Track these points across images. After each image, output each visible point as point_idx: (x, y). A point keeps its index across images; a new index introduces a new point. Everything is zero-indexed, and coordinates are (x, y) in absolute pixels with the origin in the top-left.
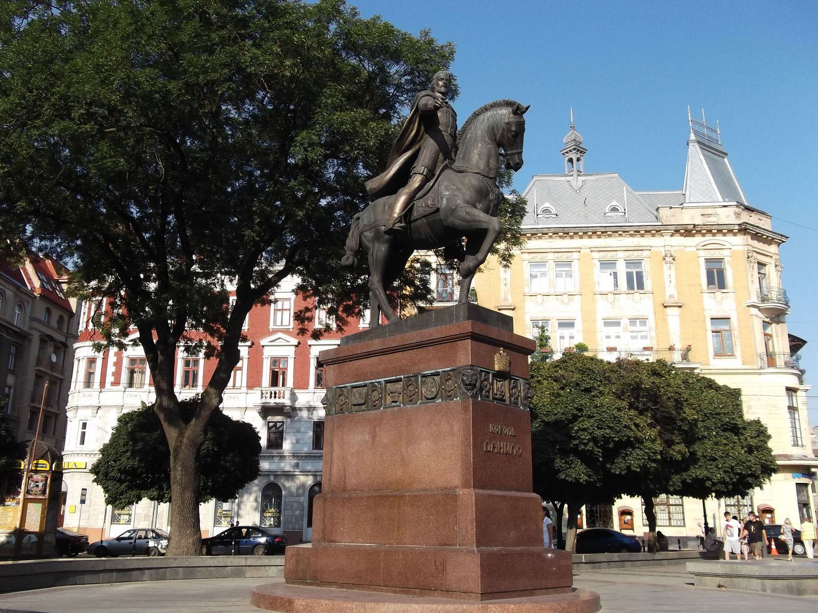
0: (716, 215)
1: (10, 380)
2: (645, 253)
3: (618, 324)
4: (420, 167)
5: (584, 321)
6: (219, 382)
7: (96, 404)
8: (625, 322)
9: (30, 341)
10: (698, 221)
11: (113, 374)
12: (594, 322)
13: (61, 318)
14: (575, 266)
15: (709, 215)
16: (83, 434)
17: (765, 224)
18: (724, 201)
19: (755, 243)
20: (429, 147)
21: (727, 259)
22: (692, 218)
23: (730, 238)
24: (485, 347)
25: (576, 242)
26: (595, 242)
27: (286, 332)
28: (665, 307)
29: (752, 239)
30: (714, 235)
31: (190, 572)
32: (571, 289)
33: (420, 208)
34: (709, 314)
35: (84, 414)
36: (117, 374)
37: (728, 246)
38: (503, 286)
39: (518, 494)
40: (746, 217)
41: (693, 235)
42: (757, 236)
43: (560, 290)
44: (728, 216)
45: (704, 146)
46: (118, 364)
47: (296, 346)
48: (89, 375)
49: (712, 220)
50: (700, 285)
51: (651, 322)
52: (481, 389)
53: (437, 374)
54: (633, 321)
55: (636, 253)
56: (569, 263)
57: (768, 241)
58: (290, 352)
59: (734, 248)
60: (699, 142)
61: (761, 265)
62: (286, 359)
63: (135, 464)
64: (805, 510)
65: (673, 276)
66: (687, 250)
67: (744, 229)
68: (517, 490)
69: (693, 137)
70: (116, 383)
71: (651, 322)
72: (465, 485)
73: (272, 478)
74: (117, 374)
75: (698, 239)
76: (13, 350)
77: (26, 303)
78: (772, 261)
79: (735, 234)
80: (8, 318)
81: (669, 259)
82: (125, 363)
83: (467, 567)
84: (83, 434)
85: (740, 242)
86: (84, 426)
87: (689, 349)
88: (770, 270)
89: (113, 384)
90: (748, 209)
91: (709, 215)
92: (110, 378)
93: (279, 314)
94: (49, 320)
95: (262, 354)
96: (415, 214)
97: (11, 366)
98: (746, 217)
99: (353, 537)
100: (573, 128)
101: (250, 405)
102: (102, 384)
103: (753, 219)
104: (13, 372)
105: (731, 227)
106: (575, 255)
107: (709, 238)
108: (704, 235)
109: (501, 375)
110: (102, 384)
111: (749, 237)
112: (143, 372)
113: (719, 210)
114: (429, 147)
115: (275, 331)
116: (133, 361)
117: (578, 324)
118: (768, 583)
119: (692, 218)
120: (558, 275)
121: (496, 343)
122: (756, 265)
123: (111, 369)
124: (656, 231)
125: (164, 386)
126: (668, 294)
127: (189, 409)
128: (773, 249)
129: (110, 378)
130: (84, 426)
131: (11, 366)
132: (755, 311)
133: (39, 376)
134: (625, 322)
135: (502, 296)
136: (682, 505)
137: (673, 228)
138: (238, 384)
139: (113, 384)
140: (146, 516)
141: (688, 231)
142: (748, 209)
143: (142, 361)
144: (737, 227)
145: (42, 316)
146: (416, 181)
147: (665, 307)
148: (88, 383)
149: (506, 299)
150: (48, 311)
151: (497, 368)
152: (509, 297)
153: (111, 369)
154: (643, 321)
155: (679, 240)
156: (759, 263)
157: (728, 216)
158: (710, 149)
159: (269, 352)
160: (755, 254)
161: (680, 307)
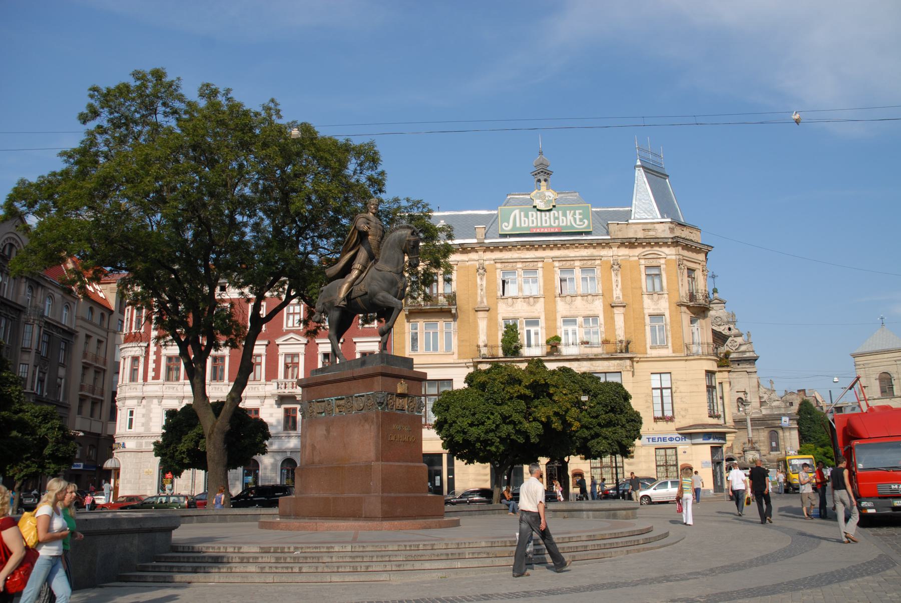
0: (655, 230)
1: (62, 372)
2: (598, 262)
3: (574, 322)
4: (357, 265)
5: (546, 319)
6: (240, 383)
7: (140, 394)
8: (580, 320)
9: (77, 337)
10: (640, 235)
11: (154, 370)
12: (555, 320)
13: (102, 315)
14: (540, 272)
15: (649, 230)
16: (131, 420)
17: (696, 237)
18: (663, 217)
19: (686, 253)
20: (363, 255)
21: (663, 267)
22: (636, 232)
23: (665, 250)
24: (390, 380)
25: (540, 253)
26: (556, 253)
27: (297, 332)
28: (613, 307)
29: (683, 249)
30: (652, 246)
31: (223, 518)
32: (535, 293)
33: (359, 290)
34: (647, 312)
35: (131, 403)
36: (157, 370)
37: (664, 256)
38: (479, 291)
39: (412, 464)
40: (678, 232)
41: (635, 247)
42: (687, 247)
43: (527, 293)
44: (664, 231)
45: (647, 170)
46: (157, 362)
47: (306, 344)
48: (134, 371)
49: (652, 234)
50: (641, 288)
51: (601, 319)
52: (387, 405)
53: (363, 396)
54: (587, 318)
55: (590, 262)
56: (535, 270)
57: (698, 251)
58: (301, 349)
59: (669, 257)
60: (643, 167)
61: (691, 271)
62: (297, 355)
63: (180, 443)
64: (718, 468)
65: (619, 279)
66: (632, 259)
67: (676, 242)
68: (412, 462)
69: (639, 163)
70: (156, 377)
71: (601, 319)
72: (377, 460)
73: (288, 455)
74: (157, 370)
75: (639, 251)
76: (63, 346)
77: (72, 304)
78: (700, 267)
79: (669, 246)
80: (58, 319)
81: (616, 267)
82: (163, 361)
83: (374, 503)
84: (131, 420)
85: (670, 253)
86: (132, 413)
87: (628, 343)
88: (699, 274)
89: (154, 378)
90: (680, 225)
91: (649, 230)
92: (151, 374)
93: (291, 317)
94: (92, 318)
95: (278, 351)
96: (353, 295)
97: (61, 360)
98: (678, 232)
99: (308, 489)
100: (541, 153)
101: (268, 394)
102: (145, 379)
103: (684, 233)
104: (63, 365)
105: (666, 241)
106: (540, 265)
107: (648, 250)
108: (644, 247)
109: (402, 396)
110: (145, 379)
111: (680, 248)
112: (178, 369)
113: (657, 226)
114: (363, 255)
115: (288, 332)
116: (170, 359)
117: (542, 322)
118: (591, 513)
119: (636, 232)
120: (526, 282)
121: (399, 377)
122: (686, 271)
123: (152, 365)
124: (606, 245)
125: (198, 386)
126: (615, 296)
127: (218, 407)
128: (701, 257)
129: (151, 374)
130: (132, 413)
131: (61, 360)
132: (684, 309)
133: (86, 367)
134: (580, 320)
135: (479, 299)
136: (657, 466)
137: (619, 241)
138: (258, 377)
139: (154, 378)
140: (186, 486)
141: (631, 244)
142: (680, 225)
143: (177, 358)
144: (670, 240)
145: (86, 314)
146: (355, 273)
147: (613, 307)
148: (133, 378)
149: (482, 302)
150: (91, 309)
151: (399, 391)
152: (485, 300)
153: (152, 365)
154: (595, 318)
155: (624, 251)
156: (688, 269)
157: (663, 231)
158: (655, 173)
159: (282, 350)
160: (685, 262)
161: (624, 306)
